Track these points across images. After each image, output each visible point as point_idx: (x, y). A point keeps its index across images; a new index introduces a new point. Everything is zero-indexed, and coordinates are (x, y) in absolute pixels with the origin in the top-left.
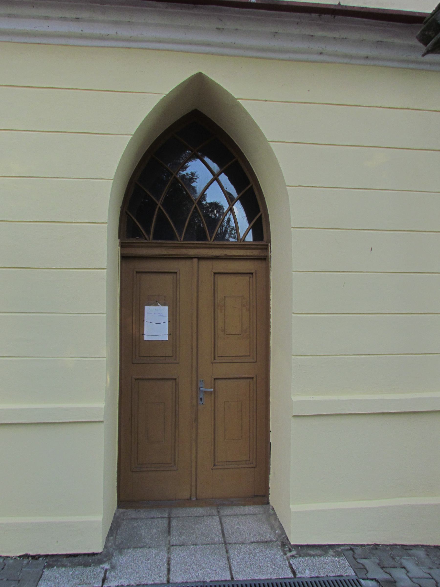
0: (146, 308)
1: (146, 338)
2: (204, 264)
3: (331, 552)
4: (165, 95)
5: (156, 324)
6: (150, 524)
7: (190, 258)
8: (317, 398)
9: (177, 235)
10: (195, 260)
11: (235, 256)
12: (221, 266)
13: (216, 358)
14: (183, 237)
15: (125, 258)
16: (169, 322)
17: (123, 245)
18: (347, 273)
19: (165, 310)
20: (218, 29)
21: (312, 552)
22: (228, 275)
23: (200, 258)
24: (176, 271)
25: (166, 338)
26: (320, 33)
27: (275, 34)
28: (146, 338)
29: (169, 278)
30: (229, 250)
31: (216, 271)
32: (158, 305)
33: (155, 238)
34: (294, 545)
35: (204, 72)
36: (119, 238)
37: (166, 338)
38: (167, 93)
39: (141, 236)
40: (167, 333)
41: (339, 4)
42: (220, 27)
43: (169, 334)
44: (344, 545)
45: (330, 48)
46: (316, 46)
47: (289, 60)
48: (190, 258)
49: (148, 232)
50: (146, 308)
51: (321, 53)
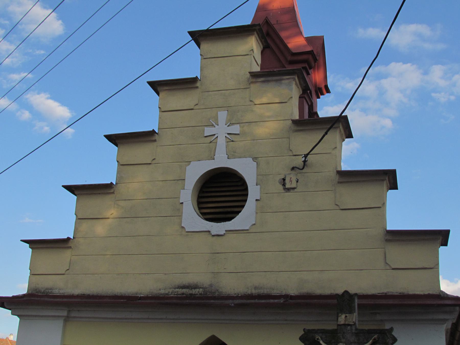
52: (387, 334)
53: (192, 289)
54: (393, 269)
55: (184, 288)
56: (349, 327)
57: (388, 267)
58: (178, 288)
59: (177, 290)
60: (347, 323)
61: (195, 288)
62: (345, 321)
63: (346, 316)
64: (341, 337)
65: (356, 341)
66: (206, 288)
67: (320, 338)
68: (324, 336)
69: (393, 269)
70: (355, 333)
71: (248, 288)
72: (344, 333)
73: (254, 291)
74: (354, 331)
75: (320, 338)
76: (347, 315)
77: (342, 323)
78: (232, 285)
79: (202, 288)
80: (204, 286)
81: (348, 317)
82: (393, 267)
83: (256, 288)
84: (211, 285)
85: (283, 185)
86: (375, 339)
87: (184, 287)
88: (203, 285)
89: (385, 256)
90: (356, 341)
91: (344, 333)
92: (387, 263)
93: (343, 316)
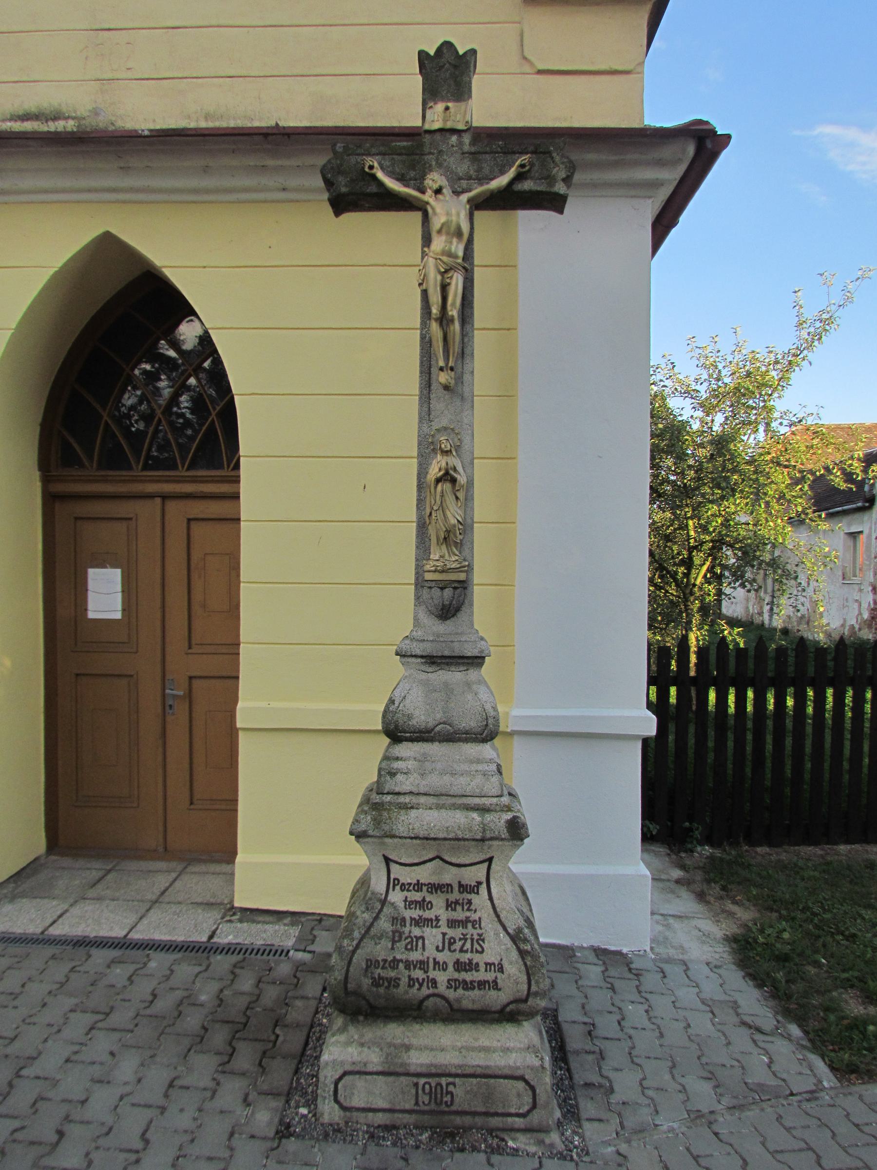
0: (91, 572)
1: (91, 615)
2: (172, 506)
3: (287, 920)
4: (56, 269)
5: (105, 594)
6: (76, 874)
7: (151, 496)
8: (275, 704)
9: (133, 462)
10: (158, 501)
11: (215, 493)
12: (198, 509)
13: (193, 646)
14: (141, 464)
15: (52, 500)
16: (123, 591)
17: (47, 479)
18: (326, 523)
19: (116, 574)
20: (121, 168)
21: (260, 919)
22: (210, 522)
23: (165, 497)
24: (131, 516)
25: (118, 616)
26: (271, 162)
27: (206, 169)
28: (91, 615)
29: (121, 527)
30: (202, 485)
31: (191, 517)
32: (105, 567)
33: (100, 467)
34: (241, 908)
35: (114, 231)
36: (40, 470)
37: (118, 616)
38: (60, 264)
39: (81, 465)
40: (120, 607)
41: (277, 124)
42: (122, 165)
43: (124, 610)
44: (313, 914)
45: (293, 182)
46: (264, 180)
47: (239, 202)
48: (151, 496)
49: (91, 458)
50: (91, 572)
51: (284, 189)
52: (554, 155)
53: (47, 122)
54: (540, 72)
55: (27, 120)
56: (454, 139)
57: (527, 68)
58: (10, 120)
59: (9, 124)
60: (449, 125)
61: (55, 118)
62: (445, 121)
63: (447, 108)
64: (434, 163)
65: (472, 172)
66: (84, 118)
67: (376, 165)
68: (387, 163)
69: (540, 72)
70: (471, 153)
71: (189, 117)
72: (440, 152)
73: (203, 124)
74: (466, 148)
75: (376, 165)
76: (450, 104)
77: (436, 126)
78: (144, 110)
79: (73, 118)
80: (79, 114)
81: (452, 110)
82: (541, 67)
83: (207, 117)
84: (96, 112)
85: (578, 1055)
86: (522, 166)
87: (26, 117)
88: (75, 112)
89: (522, 40)
90: (472, 172)
91: (440, 152)
92: (525, 58)
93: (440, 107)
